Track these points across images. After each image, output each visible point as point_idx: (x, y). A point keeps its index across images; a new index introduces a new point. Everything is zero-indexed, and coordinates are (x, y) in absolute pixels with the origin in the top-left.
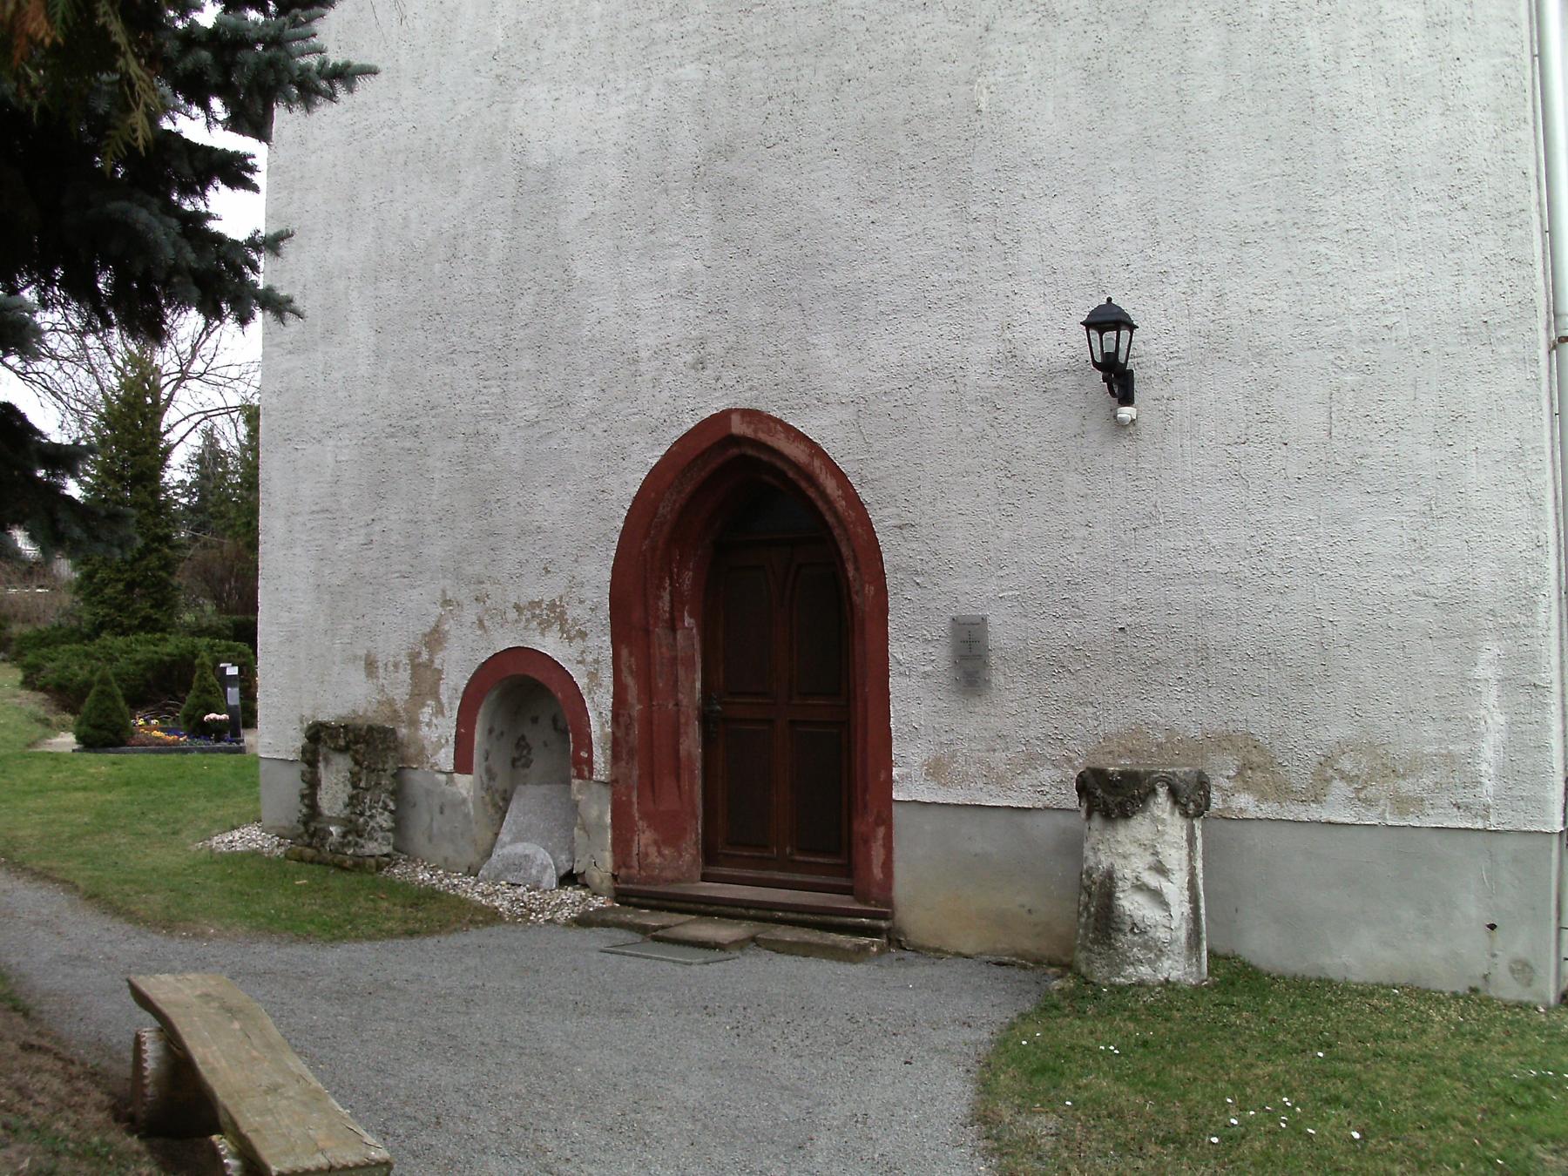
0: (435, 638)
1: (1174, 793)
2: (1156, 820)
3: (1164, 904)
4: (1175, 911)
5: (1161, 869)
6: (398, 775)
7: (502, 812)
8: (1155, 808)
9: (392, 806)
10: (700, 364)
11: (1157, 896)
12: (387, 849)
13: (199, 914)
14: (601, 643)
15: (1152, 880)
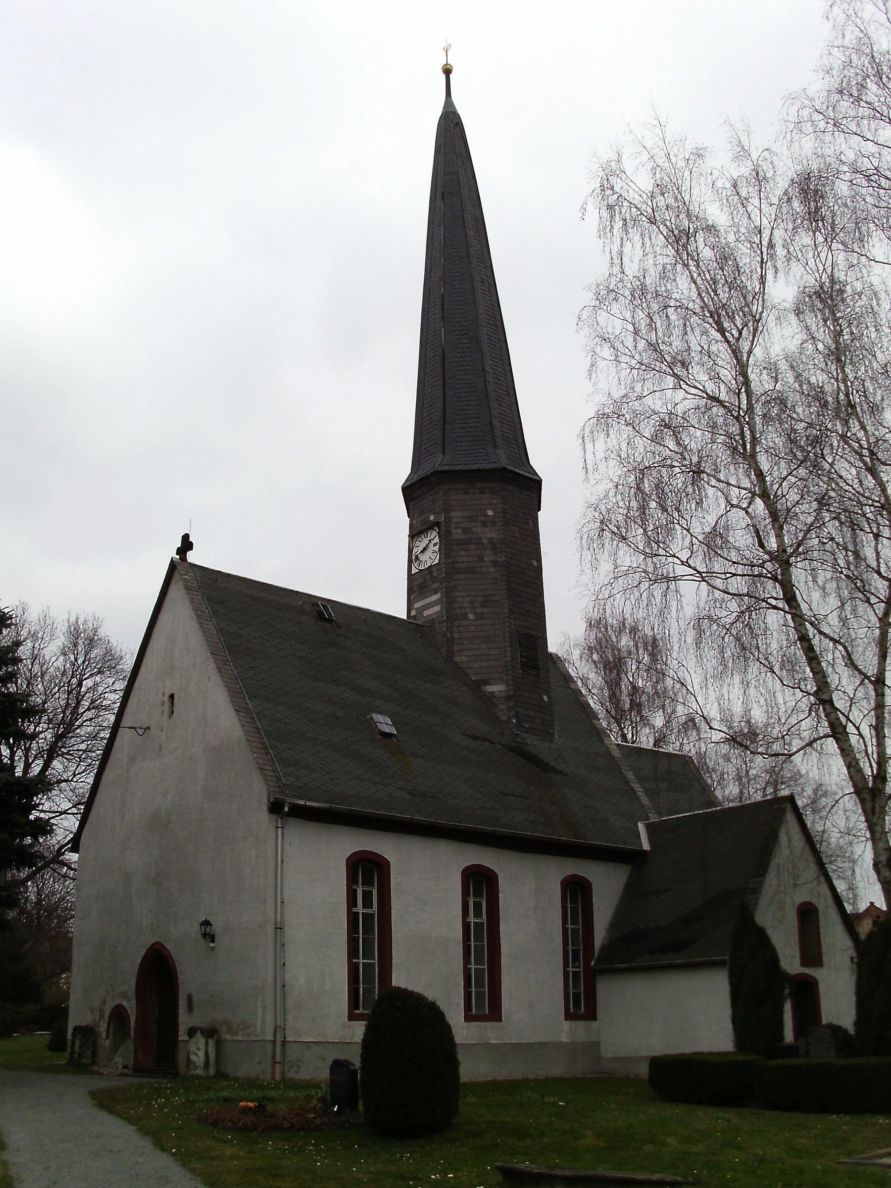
0: (104, 1002)
1: (187, 1041)
2: (198, 1038)
3: (199, 1057)
4: (201, 1059)
5: (199, 1049)
6: (95, 1041)
7: (117, 1050)
8: (737, 719)
9: (92, 1049)
10: (152, 930)
11: (197, 1054)
12: (90, 1062)
13: (798, 883)
14: (134, 1002)
15: (197, 1052)
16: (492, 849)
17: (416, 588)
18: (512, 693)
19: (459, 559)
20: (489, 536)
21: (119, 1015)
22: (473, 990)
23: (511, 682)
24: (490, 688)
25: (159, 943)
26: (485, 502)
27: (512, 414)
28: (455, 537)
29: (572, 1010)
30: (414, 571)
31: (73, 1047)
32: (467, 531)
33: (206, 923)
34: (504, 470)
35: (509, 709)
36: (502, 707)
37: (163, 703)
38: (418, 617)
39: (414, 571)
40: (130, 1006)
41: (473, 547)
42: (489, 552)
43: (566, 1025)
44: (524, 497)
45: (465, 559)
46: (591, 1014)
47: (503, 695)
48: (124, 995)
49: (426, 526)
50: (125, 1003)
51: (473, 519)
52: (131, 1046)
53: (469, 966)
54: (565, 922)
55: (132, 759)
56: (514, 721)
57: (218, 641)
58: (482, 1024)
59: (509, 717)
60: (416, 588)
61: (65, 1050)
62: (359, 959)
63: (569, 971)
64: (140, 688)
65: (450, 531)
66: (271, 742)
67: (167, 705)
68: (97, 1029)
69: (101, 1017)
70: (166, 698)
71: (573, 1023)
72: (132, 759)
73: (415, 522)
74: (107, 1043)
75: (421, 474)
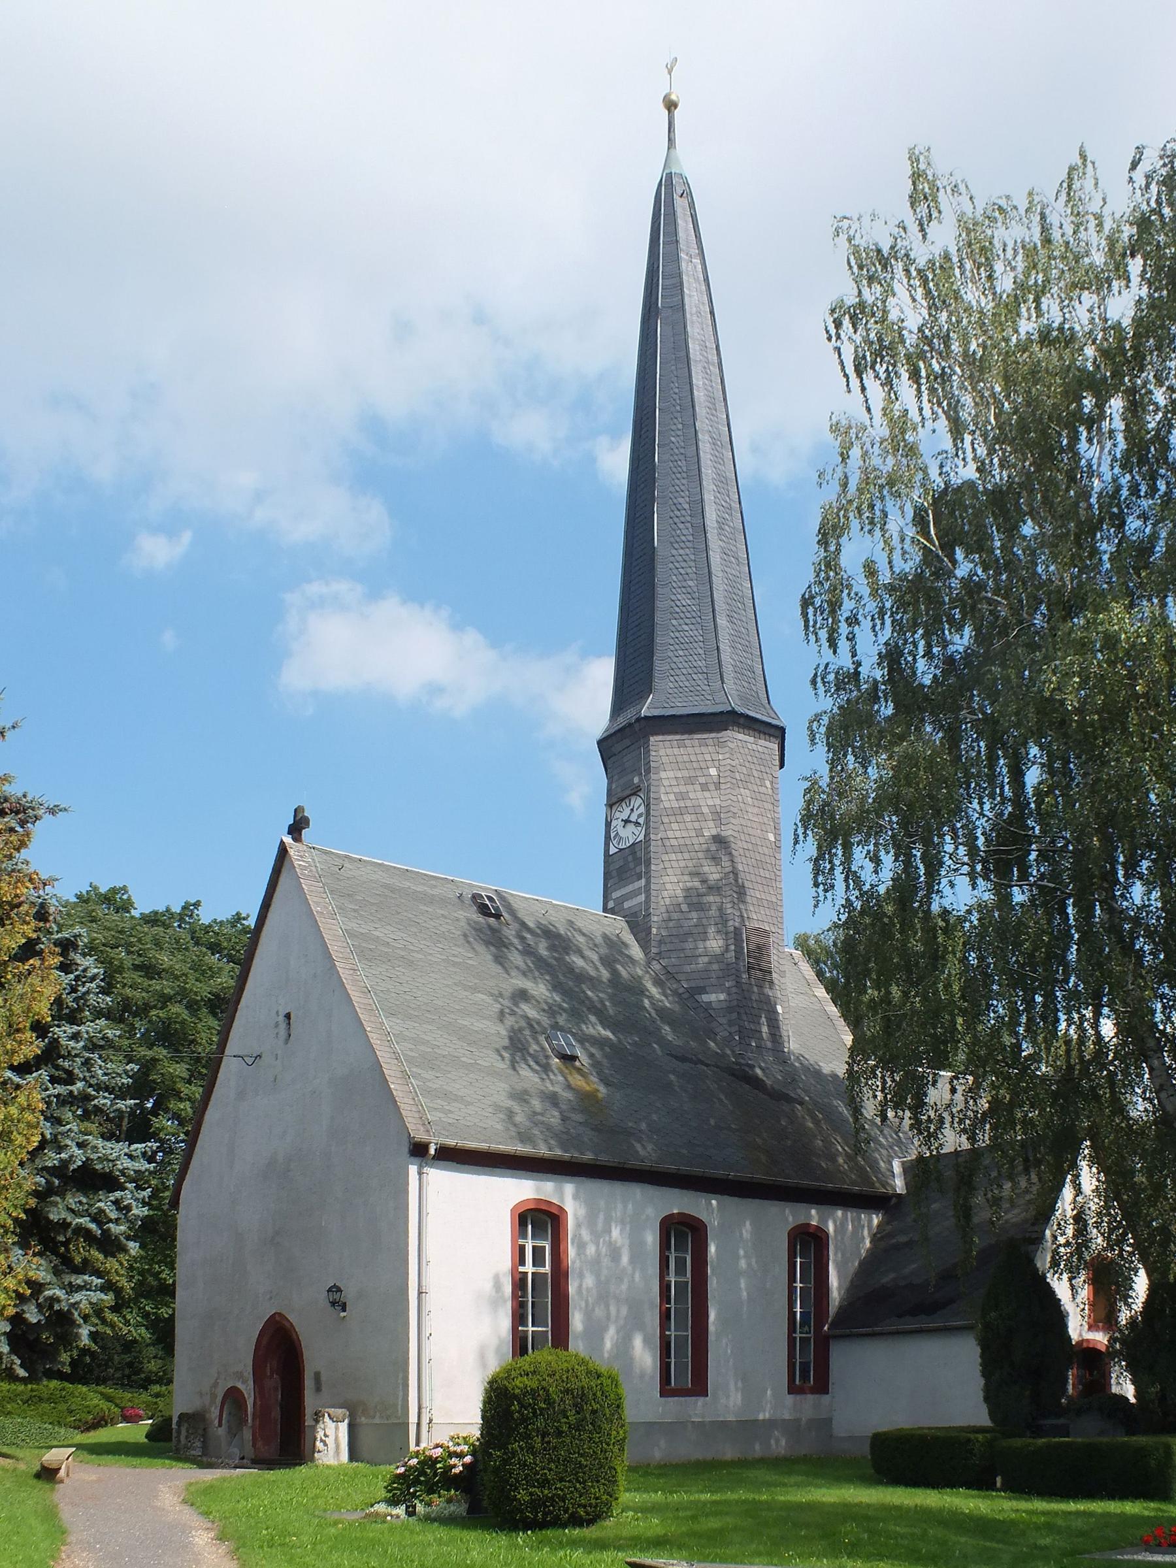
14: (251, 1383)
16: (776, 1202)
17: (614, 873)
18: (735, 1003)
19: (670, 834)
20: (710, 802)
21: (233, 1396)
22: (673, 1360)
23: (734, 990)
24: (705, 998)
25: (280, 1314)
26: (708, 757)
27: (748, 635)
28: (667, 805)
29: (797, 1382)
30: (613, 850)
31: (178, 1436)
32: (681, 796)
33: (334, 1289)
34: (733, 713)
35: (731, 1023)
36: (723, 1021)
37: (277, 1025)
38: (616, 909)
39: (613, 850)
40: (247, 1389)
41: (688, 818)
42: (711, 824)
43: (790, 1399)
44: (760, 749)
45: (678, 834)
46: (822, 1387)
47: (724, 1005)
48: (239, 1376)
49: (628, 792)
50: (240, 1385)
51: (690, 781)
52: (247, 1434)
53: (667, 1333)
54: (792, 1278)
55: (241, 1095)
56: (737, 1038)
57: (345, 944)
58: (682, 1399)
59: (730, 1033)
60: (614, 873)
61: (171, 1440)
62: (527, 1326)
63: (796, 1338)
64: (247, 1007)
65: (660, 798)
66: (414, 1070)
67: (283, 1026)
68: (207, 1416)
69: (213, 1402)
70: (281, 1018)
71: (798, 1397)
72: (241, 1095)
73: (614, 786)
74: (221, 1431)
75: (622, 721)
